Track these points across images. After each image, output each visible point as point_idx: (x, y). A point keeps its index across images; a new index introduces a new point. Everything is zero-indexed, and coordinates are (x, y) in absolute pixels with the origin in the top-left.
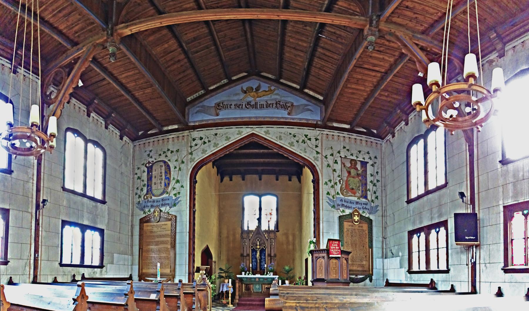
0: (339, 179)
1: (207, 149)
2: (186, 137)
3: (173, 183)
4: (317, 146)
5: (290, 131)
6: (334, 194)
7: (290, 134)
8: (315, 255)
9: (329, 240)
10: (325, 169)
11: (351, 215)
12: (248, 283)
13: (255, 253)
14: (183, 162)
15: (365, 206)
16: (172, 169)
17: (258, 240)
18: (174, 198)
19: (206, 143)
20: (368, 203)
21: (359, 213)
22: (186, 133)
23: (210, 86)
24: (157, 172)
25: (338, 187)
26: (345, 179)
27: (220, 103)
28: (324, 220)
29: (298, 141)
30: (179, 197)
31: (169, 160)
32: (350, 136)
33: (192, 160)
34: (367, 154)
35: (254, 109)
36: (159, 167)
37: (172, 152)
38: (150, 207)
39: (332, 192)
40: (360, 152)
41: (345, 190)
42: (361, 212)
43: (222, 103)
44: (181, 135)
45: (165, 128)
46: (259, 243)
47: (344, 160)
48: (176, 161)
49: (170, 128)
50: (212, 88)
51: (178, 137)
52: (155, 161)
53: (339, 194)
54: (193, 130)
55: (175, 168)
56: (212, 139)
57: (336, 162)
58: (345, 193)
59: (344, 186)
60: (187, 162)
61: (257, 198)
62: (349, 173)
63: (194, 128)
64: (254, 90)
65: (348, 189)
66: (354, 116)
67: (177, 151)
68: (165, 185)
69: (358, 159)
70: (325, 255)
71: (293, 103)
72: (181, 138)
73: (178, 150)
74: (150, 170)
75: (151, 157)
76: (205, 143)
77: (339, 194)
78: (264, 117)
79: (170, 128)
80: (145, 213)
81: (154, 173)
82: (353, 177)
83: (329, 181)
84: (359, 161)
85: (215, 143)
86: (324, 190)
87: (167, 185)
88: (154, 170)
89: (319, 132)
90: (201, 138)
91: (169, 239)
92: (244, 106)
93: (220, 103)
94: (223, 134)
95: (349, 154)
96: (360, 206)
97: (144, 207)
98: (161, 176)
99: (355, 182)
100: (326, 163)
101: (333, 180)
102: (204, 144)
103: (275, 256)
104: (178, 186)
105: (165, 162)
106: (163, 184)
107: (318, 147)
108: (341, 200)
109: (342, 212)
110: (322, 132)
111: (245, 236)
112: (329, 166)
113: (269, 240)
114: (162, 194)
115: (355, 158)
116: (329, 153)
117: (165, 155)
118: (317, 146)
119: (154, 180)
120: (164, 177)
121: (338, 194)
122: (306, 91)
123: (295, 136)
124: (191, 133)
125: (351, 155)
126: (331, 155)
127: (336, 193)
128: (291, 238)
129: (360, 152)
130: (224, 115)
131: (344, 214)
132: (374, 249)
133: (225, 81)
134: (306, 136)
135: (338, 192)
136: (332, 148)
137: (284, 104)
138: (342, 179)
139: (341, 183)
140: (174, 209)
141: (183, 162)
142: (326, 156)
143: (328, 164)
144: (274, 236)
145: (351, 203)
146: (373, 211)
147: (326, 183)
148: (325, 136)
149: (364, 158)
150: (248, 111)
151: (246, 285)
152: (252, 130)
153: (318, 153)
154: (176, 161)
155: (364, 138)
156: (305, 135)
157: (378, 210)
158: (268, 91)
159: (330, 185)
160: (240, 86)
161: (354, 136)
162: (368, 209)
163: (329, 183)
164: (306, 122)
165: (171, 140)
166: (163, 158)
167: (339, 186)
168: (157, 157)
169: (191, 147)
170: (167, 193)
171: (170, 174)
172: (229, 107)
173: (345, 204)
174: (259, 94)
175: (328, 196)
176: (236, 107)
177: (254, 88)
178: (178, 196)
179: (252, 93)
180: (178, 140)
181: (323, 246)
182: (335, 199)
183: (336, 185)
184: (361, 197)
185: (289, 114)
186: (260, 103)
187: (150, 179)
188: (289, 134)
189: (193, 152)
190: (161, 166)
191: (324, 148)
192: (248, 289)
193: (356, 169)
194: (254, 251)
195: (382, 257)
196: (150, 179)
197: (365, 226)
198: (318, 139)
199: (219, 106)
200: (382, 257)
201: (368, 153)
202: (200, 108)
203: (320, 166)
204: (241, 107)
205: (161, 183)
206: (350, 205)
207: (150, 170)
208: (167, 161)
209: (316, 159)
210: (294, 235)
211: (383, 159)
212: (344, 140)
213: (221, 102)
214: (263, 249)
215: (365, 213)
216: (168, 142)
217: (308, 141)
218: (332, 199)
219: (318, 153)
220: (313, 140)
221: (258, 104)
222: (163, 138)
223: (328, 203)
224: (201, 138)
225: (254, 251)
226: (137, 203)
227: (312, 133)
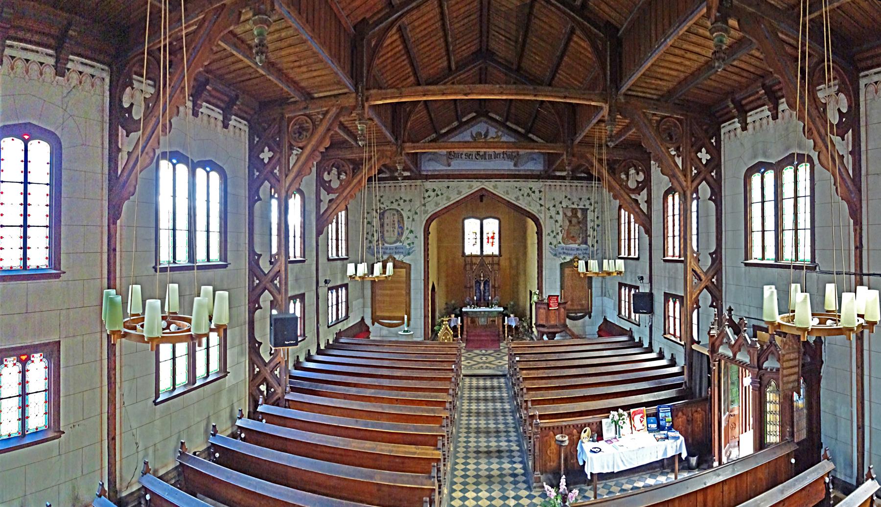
2: (418, 187)
3: (406, 233)
4: (540, 199)
5: (518, 184)
9: (549, 296)
10: (548, 220)
12: (474, 317)
14: (416, 213)
16: (405, 219)
18: (408, 247)
22: (419, 182)
23: (441, 129)
24: (389, 220)
25: (560, 237)
26: (566, 228)
28: (547, 267)
29: (523, 195)
31: (402, 210)
33: (426, 212)
39: (555, 242)
50: (443, 131)
52: (386, 208)
57: (558, 213)
59: (565, 236)
61: (478, 222)
62: (570, 222)
63: (427, 178)
65: (569, 237)
67: (411, 201)
68: (399, 234)
70: (546, 307)
72: (413, 188)
74: (382, 216)
75: (383, 203)
76: (437, 195)
78: (493, 170)
81: (386, 221)
85: (447, 197)
87: (401, 234)
88: (386, 217)
89: (542, 183)
90: (434, 190)
91: (404, 285)
92: (474, 157)
95: (571, 202)
96: (580, 252)
98: (394, 224)
99: (575, 230)
100: (548, 215)
103: (499, 287)
104: (411, 236)
105: (398, 211)
106: (396, 233)
108: (563, 249)
111: (468, 267)
112: (551, 217)
114: (395, 242)
115: (576, 207)
117: (397, 203)
118: (540, 199)
119: (386, 228)
120: (396, 225)
121: (560, 243)
122: (530, 135)
123: (520, 190)
128: (514, 262)
130: (457, 165)
132: (593, 289)
133: (456, 124)
134: (531, 189)
140: (408, 257)
141: (416, 213)
145: (572, 250)
147: (549, 234)
148: (547, 187)
149: (584, 206)
150: (478, 162)
151: (472, 318)
153: (541, 205)
155: (585, 183)
159: (552, 235)
160: (469, 131)
163: (551, 234)
166: (395, 206)
167: (561, 235)
171: (404, 224)
178: (412, 245)
184: (582, 243)
185: (515, 165)
187: (382, 225)
190: (394, 215)
192: (473, 322)
193: (577, 217)
194: (478, 282)
195: (602, 296)
196: (382, 225)
199: (450, 154)
200: (602, 296)
201: (589, 199)
203: (543, 218)
205: (393, 231)
207: (382, 216)
209: (540, 212)
210: (517, 259)
217: (533, 194)
219: (541, 205)
224: (434, 190)
225: (478, 282)
227: (536, 185)
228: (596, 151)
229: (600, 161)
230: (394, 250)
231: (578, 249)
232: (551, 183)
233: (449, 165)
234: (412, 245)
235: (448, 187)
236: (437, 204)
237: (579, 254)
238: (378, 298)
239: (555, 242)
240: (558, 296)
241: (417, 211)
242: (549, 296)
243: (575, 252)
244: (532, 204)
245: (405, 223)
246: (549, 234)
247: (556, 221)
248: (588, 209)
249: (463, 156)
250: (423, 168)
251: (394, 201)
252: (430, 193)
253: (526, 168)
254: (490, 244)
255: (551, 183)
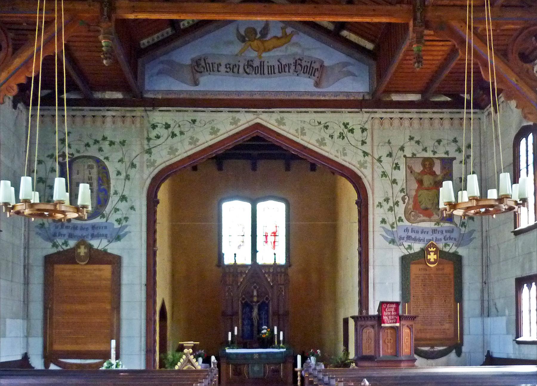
0: (403, 194)
1: (179, 146)
2: (138, 120)
3: (113, 201)
4: (363, 143)
5: (319, 117)
6: (394, 220)
7: (320, 123)
8: (359, 323)
11: (424, 252)
13: (248, 309)
14: (133, 166)
15: (448, 235)
17: (255, 287)
18: (116, 226)
19: (176, 135)
20: (455, 229)
21: (437, 248)
22: (139, 111)
25: (400, 210)
26: (413, 193)
27: (200, 60)
29: (331, 136)
30: (126, 226)
31: (107, 158)
32: (422, 116)
34: (453, 144)
35: (258, 75)
36: (86, 167)
37: (112, 143)
38: (66, 237)
40: (439, 142)
41: (413, 213)
42: (441, 246)
43: (205, 60)
44: (128, 114)
45: (99, 95)
46: (257, 292)
47: (411, 162)
48: (119, 161)
49: (109, 95)
51: (124, 117)
52: (76, 155)
53: (402, 221)
54: (151, 108)
55: (117, 175)
56: (187, 129)
58: (413, 218)
59: (411, 206)
60: (142, 167)
62: (420, 182)
64: (259, 36)
66: (428, 81)
67: (123, 143)
69: (437, 156)
71: (323, 62)
73: (124, 141)
77: (402, 221)
79: (109, 95)
80: (55, 245)
82: (428, 189)
83: (385, 200)
84: (437, 158)
86: (376, 216)
89: (366, 115)
90: (167, 126)
92: (241, 70)
93: (200, 60)
94: (207, 121)
95: (420, 148)
96: (439, 236)
97: (55, 235)
100: (379, 171)
101: (391, 198)
102: (172, 137)
104: (122, 205)
105: (98, 161)
107: (366, 143)
108: (407, 230)
109: (407, 249)
110: (373, 115)
112: (384, 174)
113: (275, 287)
116: (383, 152)
117: (97, 147)
118: (363, 143)
121: (400, 220)
123: (326, 127)
124: (148, 113)
125: (423, 150)
126: (387, 156)
127: (398, 219)
129: (439, 142)
131: (412, 252)
134: (346, 125)
135: (400, 218)
136: (389, 142)
137: (309, 65)
138: (407, 195)
139: (406, 201)
141: (133, 166)
142: (380, 157)
143: (384, 172)
144: (285, 281)
145: (423, 232)
146: (462, 241)
147: (380, 205)
148: (377, 122)
152: (255, 116)
153: (365, 154)
154: (119, 161)
155: (446, 113)
156: (344, 124)
157: (474, 238)
158: (281, 37)
159: (386, 206)
161: (429, 113)
162: (455, 239)
163: (384, 204)
164: (345, 98)
165: (109, 120)
166: (93, 151)
167: (402, 206)
168: (82, 148)
169: (149, 139)
170: (103, 216)
172: (215, 69)
173: (413, 235)
174: (266, 44)
175: (383, 225)
176: (228, 70)
177: (258, 30)
178: (124, 223)
179: (255, 42)
180: (123, 123)
181: (373, 311)
182: (395, 230)
183: (398, 206)
185: (317, 84)
186: (270, 64)
188: (317, 124)
189: (153, 150)
190: (90, 167)
191: (375, 144)
193: (433, 174)
195: (482, 314)
197: (448, 269)
198: (366, 130)
199: (198, 65)
201: (455, 141)
202: (166, 66)
203: (370, 178)
204: (236, 70)
206: (421, 236)
208: (102, 158)
211: (484, 146)
212: (411, 124)
213: (203, 57)
214: (263, 303)
215: (449, 245)
216: (104, 123)
217: (349, 135)
218: (390, 229)
219: (365, 154)
220: (358, 131)
221: (266, 63)
222: (93, 113)
223: (383, 236)
224: (167, 126)
226: (37, 227)
228: (469, 15)
229: (481, 37)
230: (90, 231)
231: (434, 231)
232: (383, 115)
233: (196, 83)
234: (124, 223)
235: (194, 121)
236: (173, 151)
237: (437, 240)
238: (56, 318)
239: (391, 218)
240: (397, 304)
241: (135, 162)
242: (382, 303)
243: (428, 237)
244: (347, 151)
245: (113, 182)
246: (380, 205)
247: (394, 182)
248: (454, 159)
249: (223, 69)
250: (147, 87)
251: (91, 142)
252: (160, 131)
253: (337, 90)
254: (270, 245)
255: (383, 115)
